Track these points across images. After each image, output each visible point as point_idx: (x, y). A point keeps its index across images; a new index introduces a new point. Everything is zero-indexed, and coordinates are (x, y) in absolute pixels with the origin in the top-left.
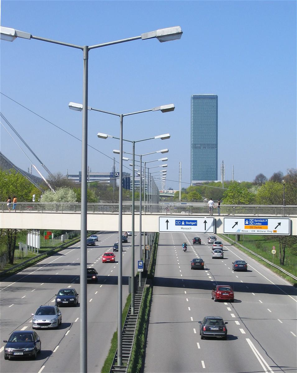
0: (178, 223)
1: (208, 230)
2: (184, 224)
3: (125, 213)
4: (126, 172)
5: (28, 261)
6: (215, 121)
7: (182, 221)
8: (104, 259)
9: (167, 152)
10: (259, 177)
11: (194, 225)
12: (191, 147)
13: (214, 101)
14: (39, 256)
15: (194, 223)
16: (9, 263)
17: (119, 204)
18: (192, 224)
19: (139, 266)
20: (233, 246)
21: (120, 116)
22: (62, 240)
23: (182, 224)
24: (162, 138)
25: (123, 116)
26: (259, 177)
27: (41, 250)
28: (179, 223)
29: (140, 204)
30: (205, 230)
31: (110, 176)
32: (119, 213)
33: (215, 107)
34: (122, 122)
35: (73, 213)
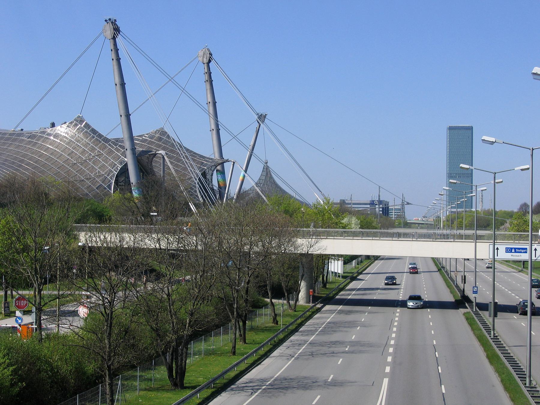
0: (508, 250)
1: (537, 258)
2: (514, 251)
3: (498, 241)
4: (385, 200)
5: (339, 286)
6: (471, 151)
7: (512, 249)
8: (386, 282)
9: (502, 182)
10: (523, 206)
11: (524, 252)
12: (447, 176)
13: (470, 132)
14: (345, 281)
15: (524, 251)
16: (323, 287)
17: (530, 233)
18: (522, 252)
19: (473, 291)
20: (520, 273)
21: (530, 149)
22: (354, 265)
23: (512, 251)
24: (522, 170)
25: (533, 149)
26: (523, 206)
27: (346, 274)
28: (509, 250)
29: (475, 232)
30: (535, 257)
31: (370, 204)
32: (529, 242)
33: (470, 137)
34: (532, 155)
35: (396, 240)
